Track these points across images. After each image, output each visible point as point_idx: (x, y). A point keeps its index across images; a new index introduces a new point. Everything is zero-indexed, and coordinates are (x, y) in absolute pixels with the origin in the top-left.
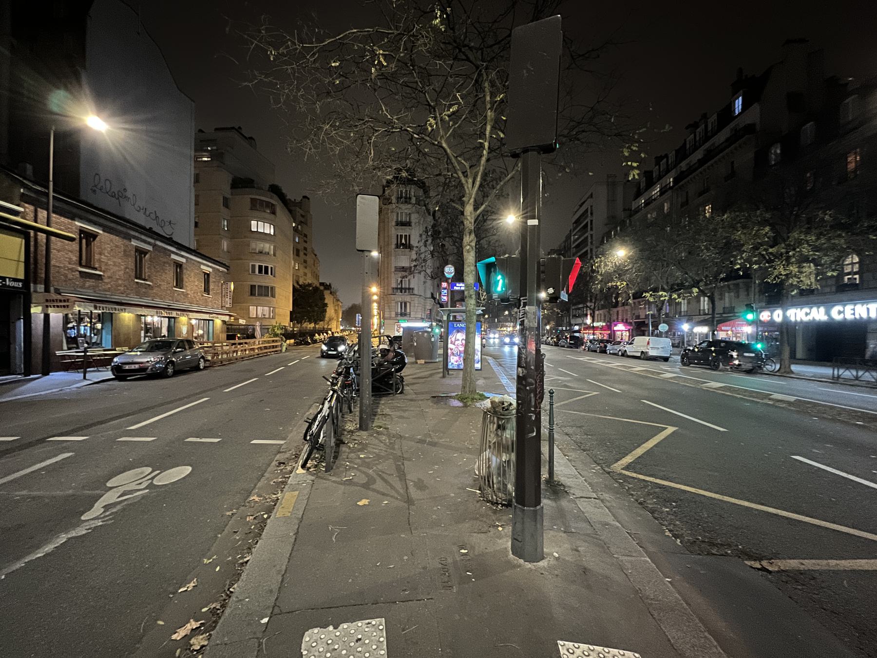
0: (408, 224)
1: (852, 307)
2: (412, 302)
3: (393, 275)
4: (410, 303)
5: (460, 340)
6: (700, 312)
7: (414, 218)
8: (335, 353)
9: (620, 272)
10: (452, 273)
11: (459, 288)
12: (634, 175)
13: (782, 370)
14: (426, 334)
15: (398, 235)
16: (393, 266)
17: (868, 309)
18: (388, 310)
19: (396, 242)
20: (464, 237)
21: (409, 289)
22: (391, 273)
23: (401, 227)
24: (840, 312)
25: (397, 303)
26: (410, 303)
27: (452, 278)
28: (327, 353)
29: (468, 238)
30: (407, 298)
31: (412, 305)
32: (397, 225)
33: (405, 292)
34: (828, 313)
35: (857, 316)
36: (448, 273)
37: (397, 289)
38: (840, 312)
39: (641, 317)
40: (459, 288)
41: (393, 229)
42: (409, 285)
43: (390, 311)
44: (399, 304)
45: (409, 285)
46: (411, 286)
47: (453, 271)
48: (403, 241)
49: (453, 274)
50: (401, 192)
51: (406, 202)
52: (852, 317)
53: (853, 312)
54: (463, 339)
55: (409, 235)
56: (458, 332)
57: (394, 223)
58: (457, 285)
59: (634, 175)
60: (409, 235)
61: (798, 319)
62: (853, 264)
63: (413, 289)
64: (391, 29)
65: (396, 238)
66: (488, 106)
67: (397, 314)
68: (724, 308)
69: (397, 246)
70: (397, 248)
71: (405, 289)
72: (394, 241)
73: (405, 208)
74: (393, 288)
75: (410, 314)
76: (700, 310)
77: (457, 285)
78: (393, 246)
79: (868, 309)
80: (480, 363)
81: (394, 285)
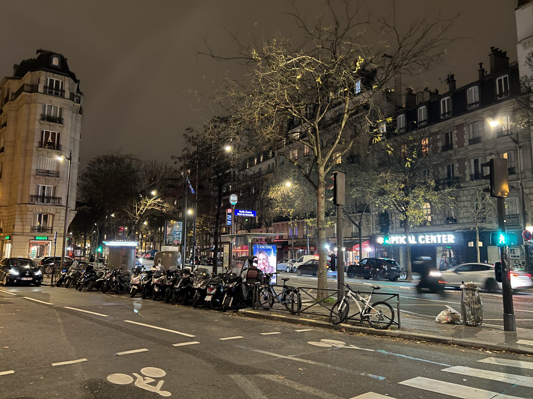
0: (59, 120)
1: (446, 236)
2: (57, 214)
3: (32, 178)
4: (53, 215)
5: (262, 259)
6: (334, 236)
7: (67, 116)
8: (30, 279)
9: (286, 198)
10: (236, 201)
11: (241, 214)
12: (408, 165)
13: (408, 278)
14: (170, 255)
15: (43, 131)
16: (34, 167)
17: (437, 238)
18: (20, 224)
19: (39, 140)
20: (320, 187)
21: (54, 198)
22: (29, 177)
23: (48, 123)
24: (423, 239)
25: (35, 215)
26: (53, 215)
27: (236, 205)
28: (21, 281)
29: (322, 189)
30: (51, 209)
31: (56, 218)
32: (43, 120)
33: (48, 202)
34: (417, 239)
35: (432, 242)
36: (233, 201)
37: (37, 197)
38: (423, 239)
39: (284, 238)
40: (241, 214)
41: (37, 122)
42: (54, 193)
43: (23, 225)
44: (38, 215)
45: (54, 193)
46: (58, 195)
47: (236, 199)
48: (50, 138)
49: (237, 202)
50: (51, 81)
51: (57, 94)
52: (429, 242)
53: (429, 239)
54: (264, 259)
55: (59, 134)
56: (260, 252)
57: (39, 117)
58: (240, 211)
59: (408, 165)
60: (59, 134)
61: (401, 243)
62: (427, 209)
63: (60, 199)
64: (319, 60)
65: (39, 134)
66: (346, 111)
67: (33, 229)
68: (352, 233)
69: (41, 145)
70: (41, 147)
71: (49, 198)
72: (37, 138)
73: (57, 102)
74: (32, 196)
75: (52, 230)
76: (334, 234)
77: (240, 211)
78: (36, 144)
79: (437, 238)
80: (276, 278)
81: (33, 192)
